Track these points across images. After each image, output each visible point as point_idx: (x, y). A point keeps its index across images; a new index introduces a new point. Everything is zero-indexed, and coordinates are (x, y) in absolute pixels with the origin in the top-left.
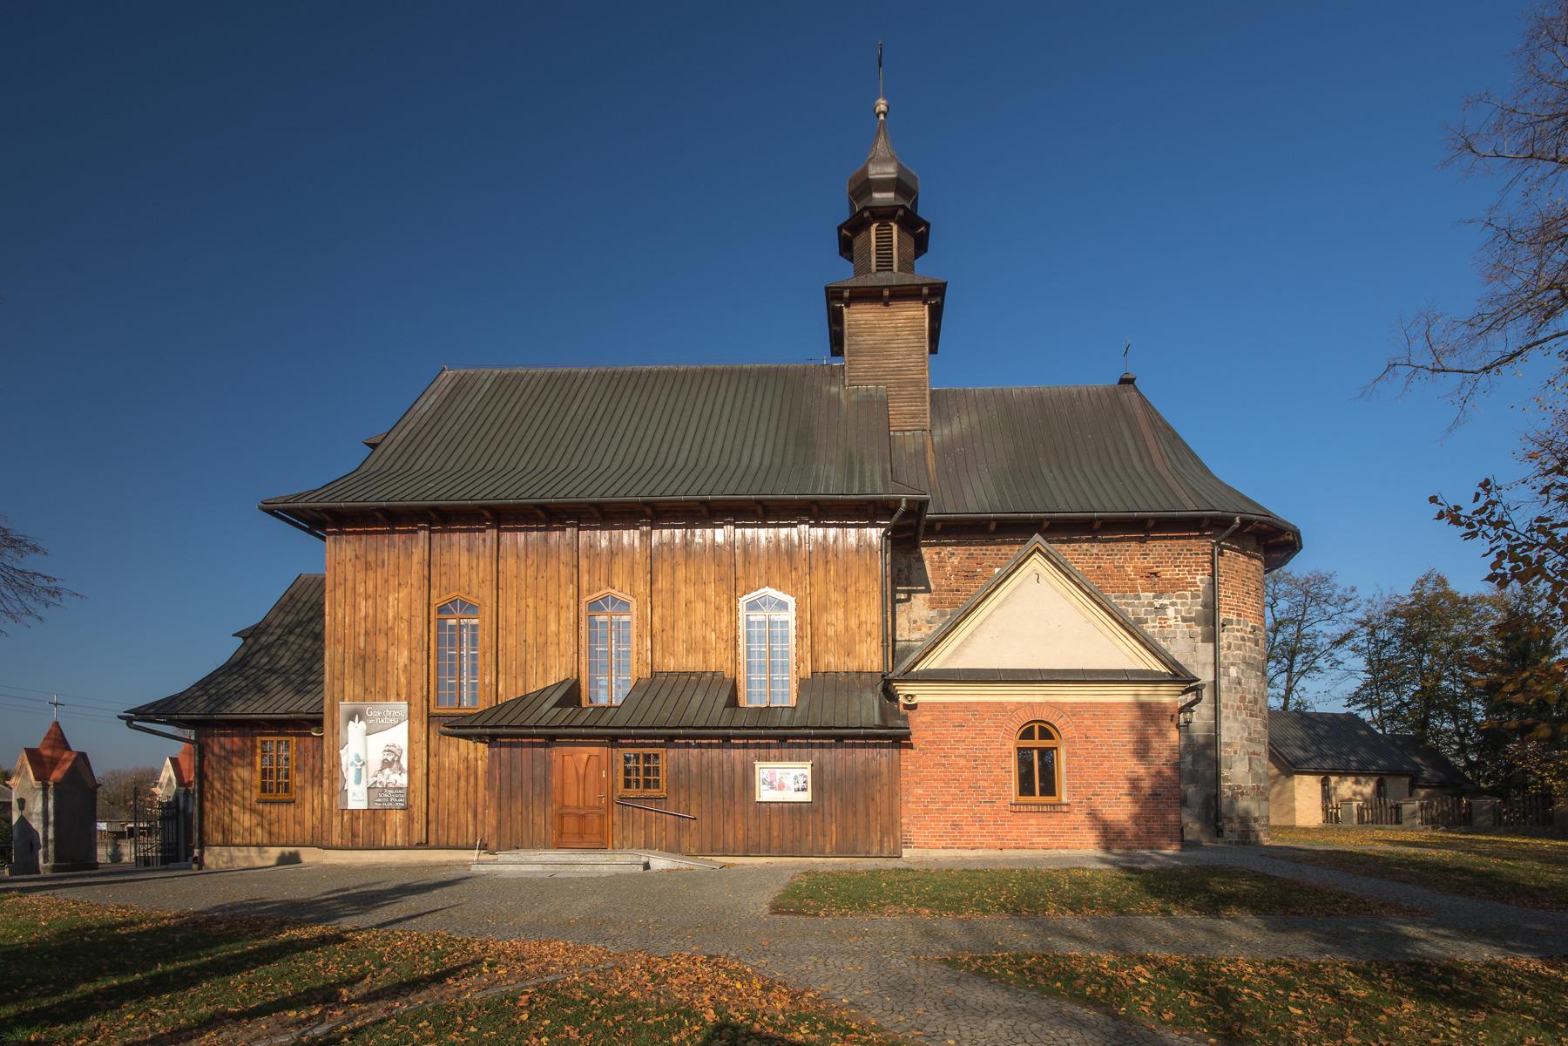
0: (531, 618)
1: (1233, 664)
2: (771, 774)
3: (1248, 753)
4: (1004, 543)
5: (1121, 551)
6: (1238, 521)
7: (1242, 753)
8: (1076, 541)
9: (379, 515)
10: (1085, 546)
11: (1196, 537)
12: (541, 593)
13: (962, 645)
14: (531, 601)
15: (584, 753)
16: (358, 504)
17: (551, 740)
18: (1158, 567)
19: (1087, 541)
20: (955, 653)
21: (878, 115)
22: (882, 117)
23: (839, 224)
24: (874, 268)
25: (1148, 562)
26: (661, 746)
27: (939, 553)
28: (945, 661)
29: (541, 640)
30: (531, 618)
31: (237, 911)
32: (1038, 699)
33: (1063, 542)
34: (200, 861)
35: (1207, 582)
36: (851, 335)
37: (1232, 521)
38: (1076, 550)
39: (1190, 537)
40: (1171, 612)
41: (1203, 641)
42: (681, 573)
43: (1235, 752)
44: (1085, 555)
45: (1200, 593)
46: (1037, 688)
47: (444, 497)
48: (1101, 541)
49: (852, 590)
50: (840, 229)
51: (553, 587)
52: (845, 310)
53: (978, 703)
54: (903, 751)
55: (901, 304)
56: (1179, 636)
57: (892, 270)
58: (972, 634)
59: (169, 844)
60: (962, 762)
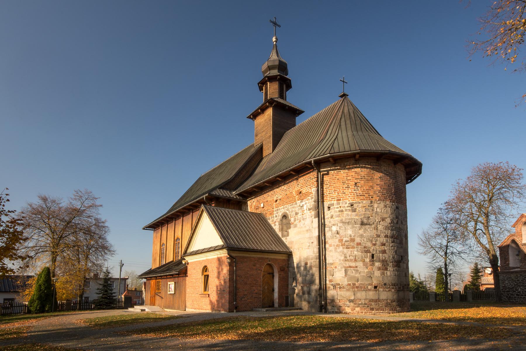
1: (334, 225)
3: (345, 267)
5: (291, 186)
7: (340, 268)
9: (291, 172)
16: (321, 157)
18: (301, 189)
23: (258, 82)
25: (299, 188)
27: (251, 202)
31: (77, 330)
34: (134, 307)
35: (315, 191)
38: (280, 190)
39: (310, 172)
40: (305, 207)
41: (315, 218)
43: (336, 267)
44: (283, 191)
45: (313, 196)
47: (317, 155)
50: (258, 84)
56: (308, 217)
59: (120, 306)
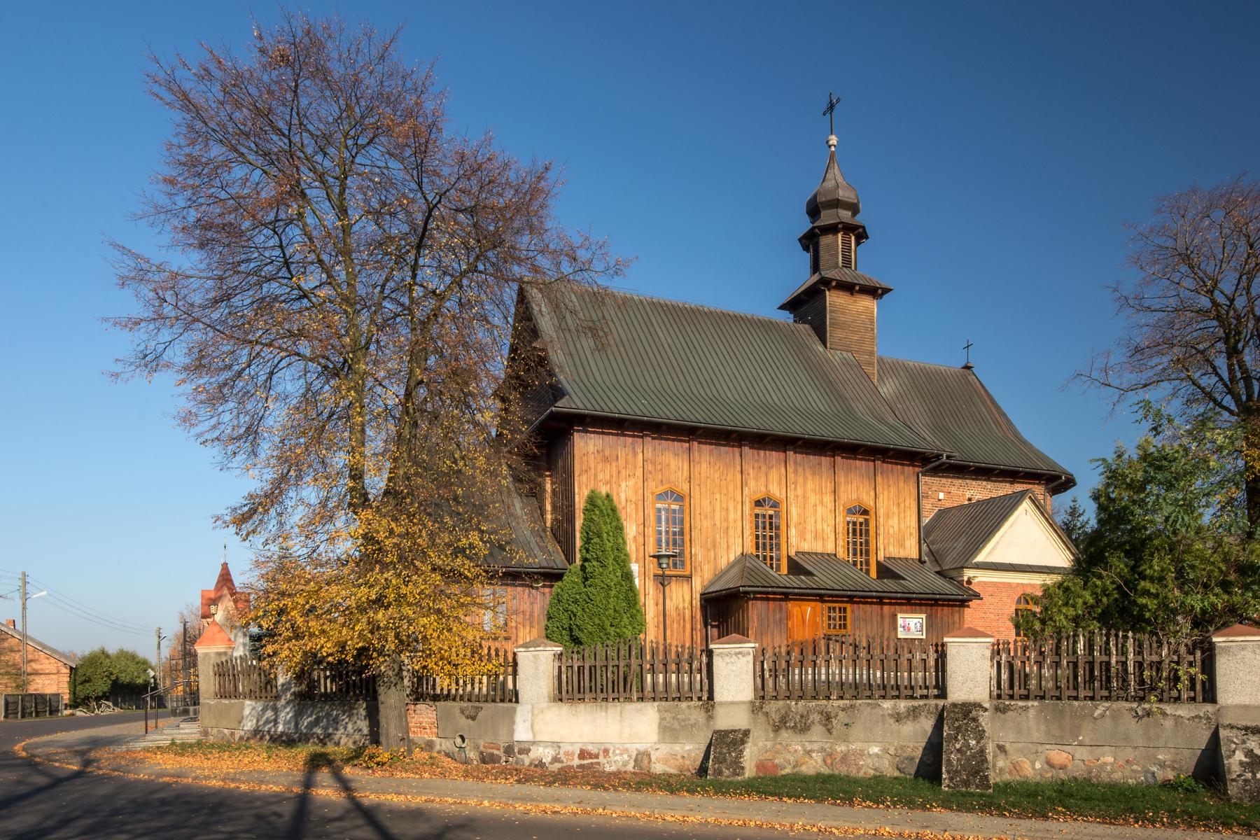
0: (718, 508)
2: (904, 621)
4: (943, 477)
6: (1063, 478)
8: (980, 480)
10: (984, 483)
11: (1037, 484)
12: (724, 491)
13: (993, 549)
14: (718, 496)
15: (809, 609)
17: (786, 597)
19: (984, 480)
20: (990, 553)
21: (830, 146)
22: (833, 149)
24: (840, 264)
26: (846, 602)
28: (985, 558)
29: (725, 524)
30: (718, 508)
32: (1026, 582)
33: (973, 479)
36: (831, 311)
37: (1061, 478)
42: (810, 485)
46: (1027, 575)
48: (992, 481)
49: (902, 505)
51: (731, 488)
52: (827, 292)
53: (1000, 583)
54: (966, 609)
55: (864, 297)
57: (850, 268)
58: (997, 543)
60: (992, 616)
